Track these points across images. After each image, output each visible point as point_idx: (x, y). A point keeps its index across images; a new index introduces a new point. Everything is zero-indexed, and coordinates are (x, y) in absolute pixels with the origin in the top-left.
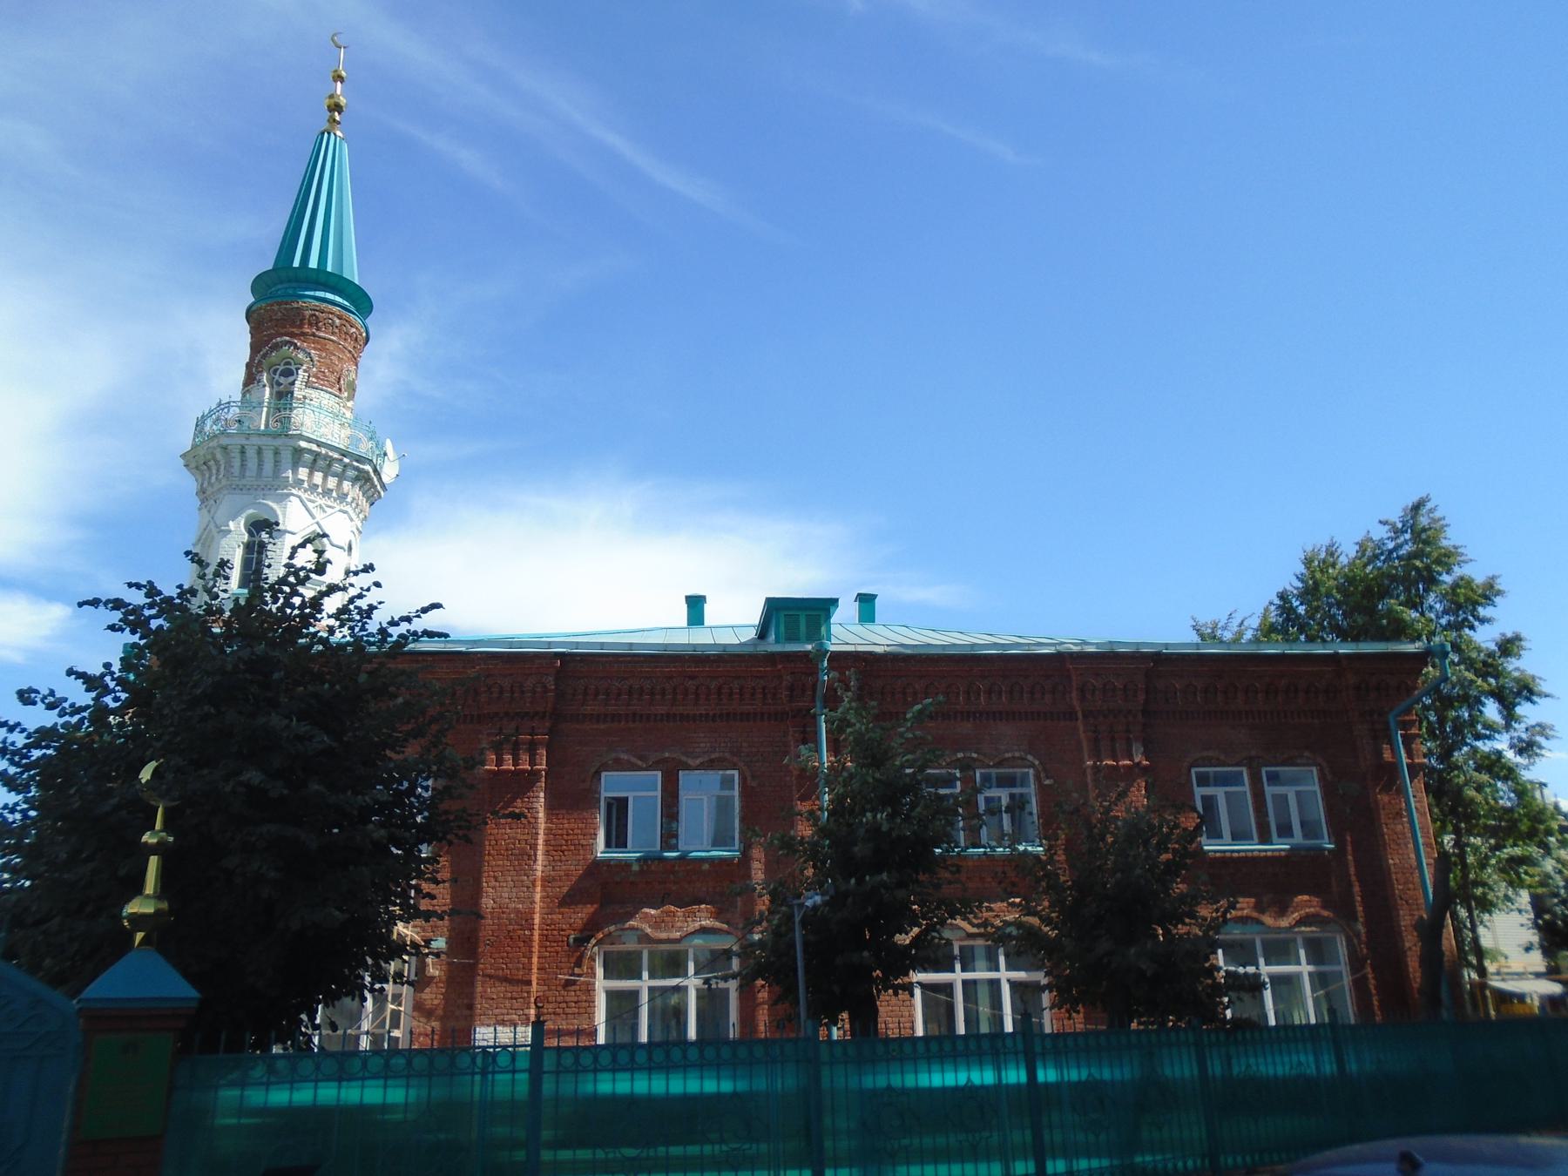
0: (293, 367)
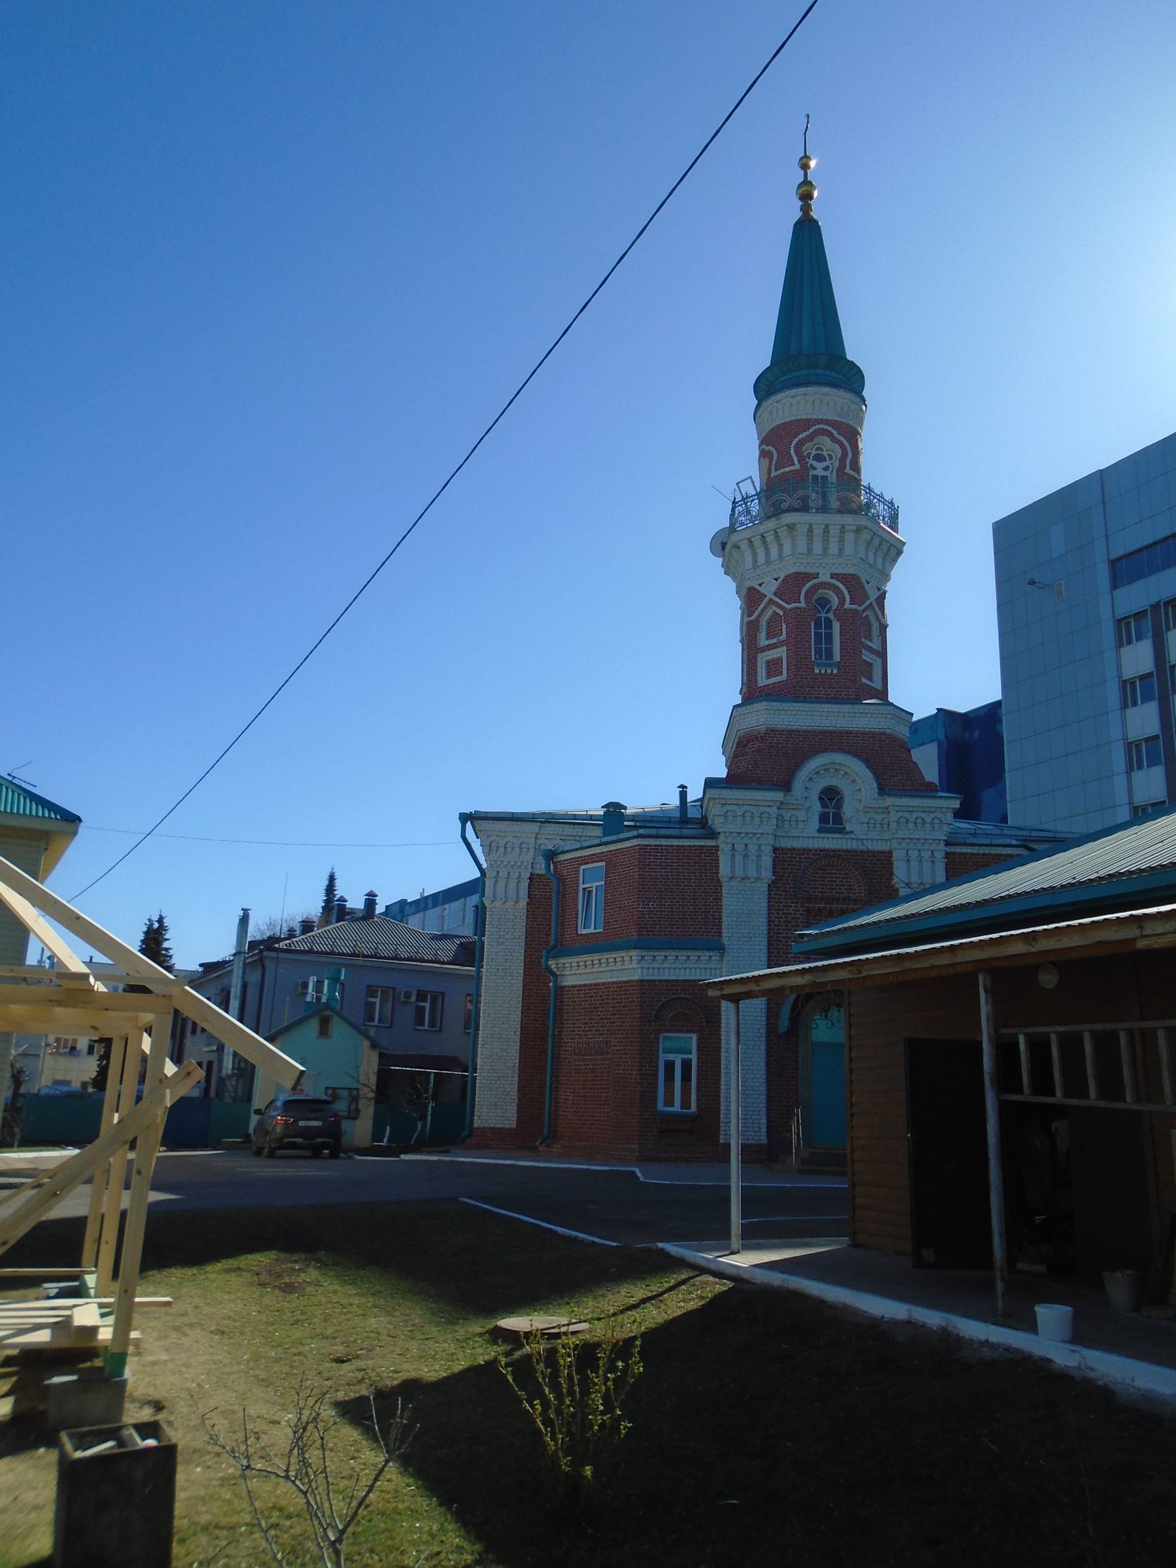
0: (825, 453)
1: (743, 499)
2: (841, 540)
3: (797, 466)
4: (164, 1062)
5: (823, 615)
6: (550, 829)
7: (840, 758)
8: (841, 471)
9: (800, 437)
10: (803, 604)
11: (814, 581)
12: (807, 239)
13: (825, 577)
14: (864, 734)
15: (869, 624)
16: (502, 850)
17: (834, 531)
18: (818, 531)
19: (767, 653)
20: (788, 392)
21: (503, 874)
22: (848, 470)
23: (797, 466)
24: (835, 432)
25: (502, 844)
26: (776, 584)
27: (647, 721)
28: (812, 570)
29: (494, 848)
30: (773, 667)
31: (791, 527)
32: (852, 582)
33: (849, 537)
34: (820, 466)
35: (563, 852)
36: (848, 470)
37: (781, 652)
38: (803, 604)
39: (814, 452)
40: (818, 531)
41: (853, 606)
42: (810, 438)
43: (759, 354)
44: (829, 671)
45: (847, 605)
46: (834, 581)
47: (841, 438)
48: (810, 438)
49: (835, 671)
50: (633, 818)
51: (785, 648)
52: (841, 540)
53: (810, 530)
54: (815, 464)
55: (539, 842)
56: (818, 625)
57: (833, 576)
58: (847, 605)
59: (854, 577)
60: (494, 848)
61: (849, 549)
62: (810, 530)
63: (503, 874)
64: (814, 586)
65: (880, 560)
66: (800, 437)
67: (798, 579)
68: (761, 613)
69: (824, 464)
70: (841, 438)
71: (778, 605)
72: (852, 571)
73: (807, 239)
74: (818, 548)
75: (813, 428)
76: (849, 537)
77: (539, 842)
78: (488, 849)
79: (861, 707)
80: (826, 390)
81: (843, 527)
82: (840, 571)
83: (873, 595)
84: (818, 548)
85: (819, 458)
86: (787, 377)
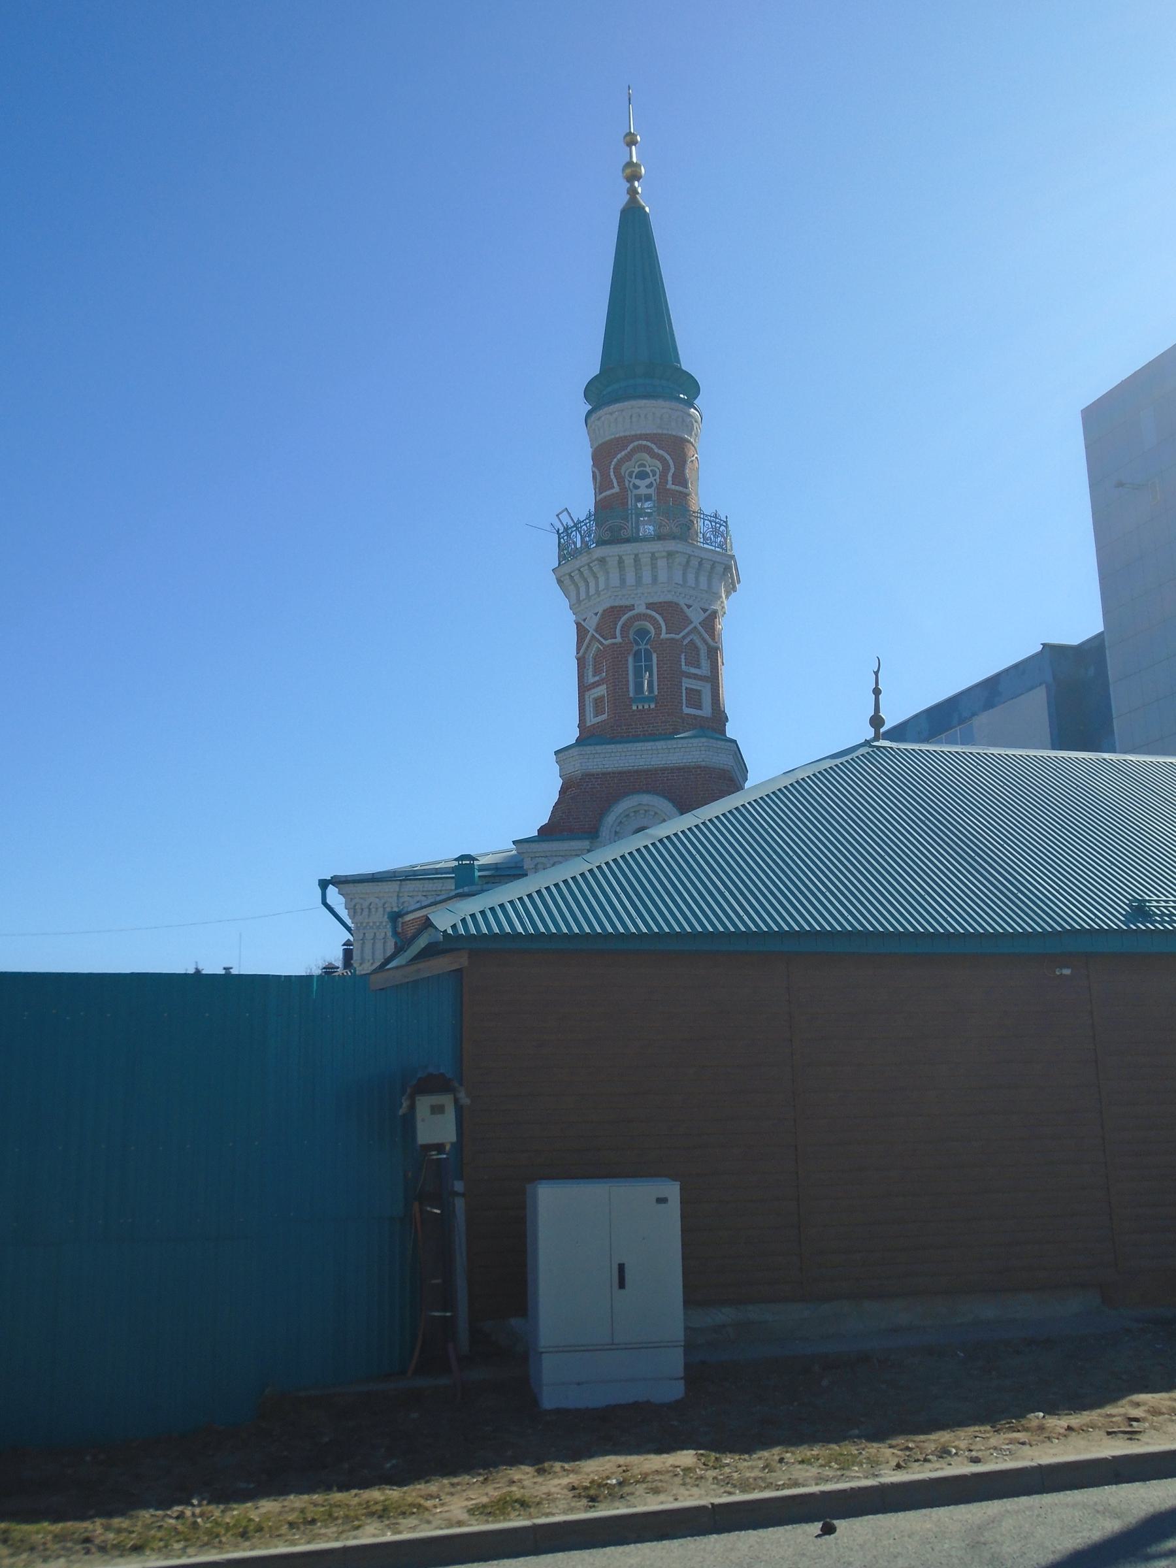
0: (648, 469)
1: (575, 525)
2: (654, 567)
3: (616, 489)
4: (819, 1521)
5: (642, 647)
6: (410, 886)
7: (646, 799)
8: (662, 490)
9: (619, 456)
10: (619, 640)
11: (631, 614)
12: (634, 228)
13: (641, 609)
14: (679, 769)
15: (697, 649)
16: (366, 912)
17: (645, 560)
18: (629, 561)
19: (593, 691)
20: (606, 409)
21: (369, 936)
22: (670, 486)
23: (616, 489)
24: (654, 446)
25: (366, 904)
26: (596, 619)
27: (470, 770)
28: (628, 603)
29: (359, 911)
30: (598, 701)
31: (602, 561)
32: (671, 612)
33: (662, 563)
34: (642, 484)
35: (408, 913)
36: (670, 486)
37: (601, 690)
38: (619, 640)
39: (637, 470)
40: (629, 561)
41: (669, 636)
42: (628, 457)
43: (586, 358)
44: (646, 707)
45: (664, 636)
46: (649, 612)
47: (661, 452)
48: (628, 457)
49: (653, 706)
50: (483, 868)
51: (605, 686)
52: (654, 567)
53: (621, 561)
54: (638, 482)
55: (402, 900)
56: (637, 655)
57: (649, 606)
58: (664, 636)
59: (670, 604)
60: (359, 911)
61: (662, 576)
62: (621, 561)
63: (369, 936)
64: (630, 618)
65: (703, 579)
66: (619, 456)
67: (614, 613)
68: (587, 649)
69: (647, 481)
70: (661, 452)
71: (598, 641)
72: (669, 598)
73: (634, 228)
74: (630, 578)
75: (632, 446)
76: (662, 563)
77: (402, 900)
78: (353, 910)
79: (674, 742)
80: (643, 402)
81: (653, 554)
82: (656, 599)
83: (696, 617)
84: (630, 578)
85: (642, 475)
86: (609, 389)
